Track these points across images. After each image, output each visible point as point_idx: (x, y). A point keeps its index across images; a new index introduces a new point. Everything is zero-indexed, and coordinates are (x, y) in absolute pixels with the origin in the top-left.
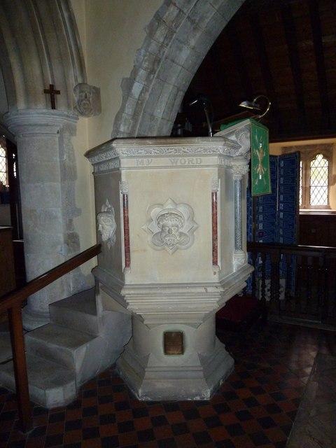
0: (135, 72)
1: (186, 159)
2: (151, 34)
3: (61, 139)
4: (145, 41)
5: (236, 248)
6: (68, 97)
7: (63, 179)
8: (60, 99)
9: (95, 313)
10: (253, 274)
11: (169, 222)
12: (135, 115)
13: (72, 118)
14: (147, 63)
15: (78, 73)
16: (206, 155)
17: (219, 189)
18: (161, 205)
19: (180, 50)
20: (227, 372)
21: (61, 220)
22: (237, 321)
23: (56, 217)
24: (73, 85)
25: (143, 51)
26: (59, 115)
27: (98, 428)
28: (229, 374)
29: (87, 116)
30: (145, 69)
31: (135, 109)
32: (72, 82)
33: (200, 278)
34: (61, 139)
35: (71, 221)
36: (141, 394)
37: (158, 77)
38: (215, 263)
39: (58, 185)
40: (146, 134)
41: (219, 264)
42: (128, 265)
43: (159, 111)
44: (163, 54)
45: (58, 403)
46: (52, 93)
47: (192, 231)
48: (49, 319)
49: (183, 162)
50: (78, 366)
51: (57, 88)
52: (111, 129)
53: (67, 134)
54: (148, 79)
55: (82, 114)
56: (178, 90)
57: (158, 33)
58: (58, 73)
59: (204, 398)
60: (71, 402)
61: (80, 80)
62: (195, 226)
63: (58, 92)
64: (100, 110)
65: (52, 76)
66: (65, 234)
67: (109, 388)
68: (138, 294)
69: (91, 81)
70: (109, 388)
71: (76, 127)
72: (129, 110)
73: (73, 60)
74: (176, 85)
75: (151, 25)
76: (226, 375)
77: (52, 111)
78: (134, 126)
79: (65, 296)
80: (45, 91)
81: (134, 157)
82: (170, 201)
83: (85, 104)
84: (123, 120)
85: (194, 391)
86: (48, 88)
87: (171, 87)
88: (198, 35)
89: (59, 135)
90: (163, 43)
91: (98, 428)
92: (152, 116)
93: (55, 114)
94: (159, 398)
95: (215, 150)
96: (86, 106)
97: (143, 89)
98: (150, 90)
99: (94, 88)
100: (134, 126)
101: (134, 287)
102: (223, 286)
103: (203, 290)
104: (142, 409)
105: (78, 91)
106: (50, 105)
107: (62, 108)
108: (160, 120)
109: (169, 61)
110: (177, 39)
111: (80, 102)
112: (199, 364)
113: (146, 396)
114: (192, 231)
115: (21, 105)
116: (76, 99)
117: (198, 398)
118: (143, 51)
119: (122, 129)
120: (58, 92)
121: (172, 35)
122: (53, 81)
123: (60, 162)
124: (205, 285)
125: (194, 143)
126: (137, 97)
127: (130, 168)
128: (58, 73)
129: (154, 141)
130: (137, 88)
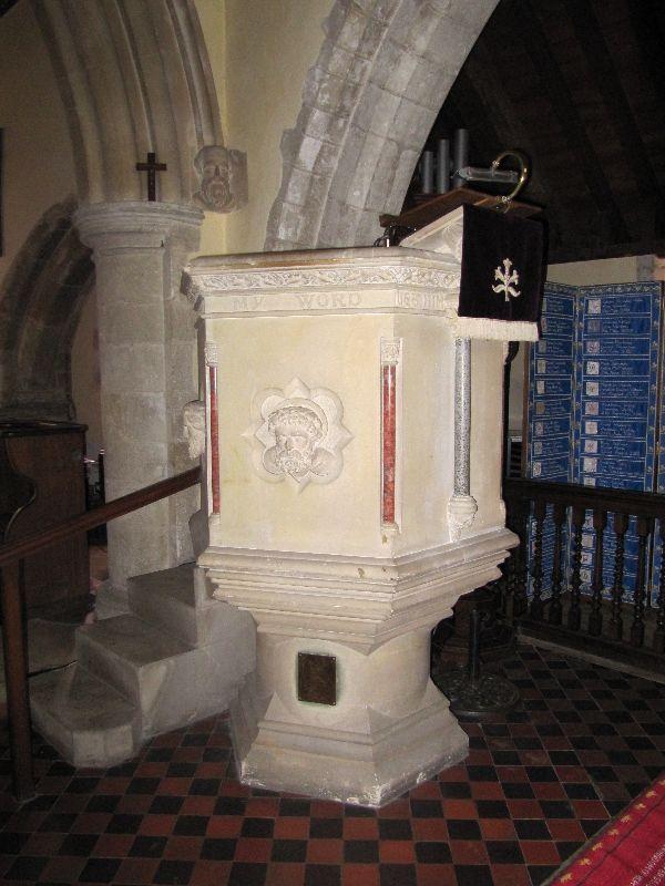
0: (304, 117)
1: (329, 294)
2: (333, 34)
3: (167, 257)
4: (321, 54)
5: (457, 490)
6: (181, 176)
7: (168, 339)
8: (167, 180)
9: (191, 602)
10: (517, 554)
11: (288, 425)
12: (309, 206)
13: (193, 216)
14: (327, 96)
15: (205, 126)
16: (369, 286)
17: (400, 360)
18: (279, 390)
19: (396, 60)
20: (442, 761)
21: (163, 417)
22: (474, 643)
23: (154, 411)
24: (193, 149)
25: (318, 71)
26: (162, 211)
27: (208, 818)
28: (447, 766)
29: (223, 210)
30: (325, 109)
31: (309, 191)
32: (192, 144)
33: (354, 546)
34: (167, 257)
35: (181, 421)
36: (249, 771)
37: (354, 125)
38: (388, 517)
39: (160, 348)
40: (332, 244)
41: (397, 519)
42: (216, 509)
43: (357, 193)
44: (362, 74)
45: (94, 762)
46: (151, 168)
47: (342, 446)
48: (127, 607)
49: (322, 302)
50: (146, 698)
51: (161, 160)
52: (264, 235)
53: (177, 249)
54: (331, 126)
55: (211, 207)
56: (401, 147)
57: (347, 29)
58: (163, 132)
59: (367, 802)
60: (121, 762)
61: (208, 140)
62: (349, 436)
63: (163, 167)
64: (246, 200)
65: (154, 138)
66: (170, 445)
67: (206, 745)
68: (227, 568)
69: (228, 137)
70: (206, 745)
71: (198, 232)
72: (295, 196)
73: (194, 102)
74: (392, 136)
75: (334, 15)
76: (438, 768)
77: (148, 205)
78: (308, 229)
79: (167, 567)
80: (139, 167)
81: (227, 292)
82: (296, 382)
83: (215, 187)
84: (284, 215)
85: (347, 784)
86: (144, 160)
87: (381, 142)
88: (432, 27)
89: (164, 251)
90: (359, 50)
91: (208, 818)
92: (344, 207)
93: (154, 211)
94: (280, 785)
95: (385, 275)
96: (217, 192)
97: (322, 151)
98: (340, 151)
99: (237, 153)
100: (308, 229)
101: (228, 553)
102: (397, 569)
103: (356, 573)
104: (236, 801)
105: (201, 163)
106: (146, 193)
107: (170, 199)
108: (360, 212)
109: (374, 87)
110: (391, 40)
111: (206, 181)
112: (366, 729)
113: (253, 776)
114: (342, 446)
115: (97, 195)
116: (199, 177)
117: (355, 801)
118: (318, 71)
119: (282, 234)
120: (163, 167)
121: (380, 31)
122: (155, 146)
123: (165, 302)
124: (361, 564)
125: (332, 262)
126: (310, 168)
127: (219, 314)
128: (163, 132)
129: (260, 260)
130: (309, 150)
